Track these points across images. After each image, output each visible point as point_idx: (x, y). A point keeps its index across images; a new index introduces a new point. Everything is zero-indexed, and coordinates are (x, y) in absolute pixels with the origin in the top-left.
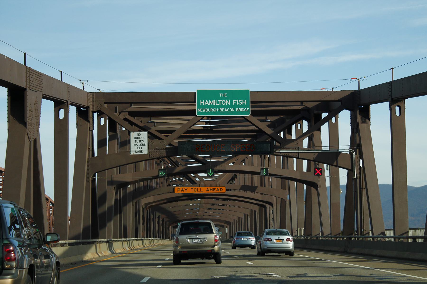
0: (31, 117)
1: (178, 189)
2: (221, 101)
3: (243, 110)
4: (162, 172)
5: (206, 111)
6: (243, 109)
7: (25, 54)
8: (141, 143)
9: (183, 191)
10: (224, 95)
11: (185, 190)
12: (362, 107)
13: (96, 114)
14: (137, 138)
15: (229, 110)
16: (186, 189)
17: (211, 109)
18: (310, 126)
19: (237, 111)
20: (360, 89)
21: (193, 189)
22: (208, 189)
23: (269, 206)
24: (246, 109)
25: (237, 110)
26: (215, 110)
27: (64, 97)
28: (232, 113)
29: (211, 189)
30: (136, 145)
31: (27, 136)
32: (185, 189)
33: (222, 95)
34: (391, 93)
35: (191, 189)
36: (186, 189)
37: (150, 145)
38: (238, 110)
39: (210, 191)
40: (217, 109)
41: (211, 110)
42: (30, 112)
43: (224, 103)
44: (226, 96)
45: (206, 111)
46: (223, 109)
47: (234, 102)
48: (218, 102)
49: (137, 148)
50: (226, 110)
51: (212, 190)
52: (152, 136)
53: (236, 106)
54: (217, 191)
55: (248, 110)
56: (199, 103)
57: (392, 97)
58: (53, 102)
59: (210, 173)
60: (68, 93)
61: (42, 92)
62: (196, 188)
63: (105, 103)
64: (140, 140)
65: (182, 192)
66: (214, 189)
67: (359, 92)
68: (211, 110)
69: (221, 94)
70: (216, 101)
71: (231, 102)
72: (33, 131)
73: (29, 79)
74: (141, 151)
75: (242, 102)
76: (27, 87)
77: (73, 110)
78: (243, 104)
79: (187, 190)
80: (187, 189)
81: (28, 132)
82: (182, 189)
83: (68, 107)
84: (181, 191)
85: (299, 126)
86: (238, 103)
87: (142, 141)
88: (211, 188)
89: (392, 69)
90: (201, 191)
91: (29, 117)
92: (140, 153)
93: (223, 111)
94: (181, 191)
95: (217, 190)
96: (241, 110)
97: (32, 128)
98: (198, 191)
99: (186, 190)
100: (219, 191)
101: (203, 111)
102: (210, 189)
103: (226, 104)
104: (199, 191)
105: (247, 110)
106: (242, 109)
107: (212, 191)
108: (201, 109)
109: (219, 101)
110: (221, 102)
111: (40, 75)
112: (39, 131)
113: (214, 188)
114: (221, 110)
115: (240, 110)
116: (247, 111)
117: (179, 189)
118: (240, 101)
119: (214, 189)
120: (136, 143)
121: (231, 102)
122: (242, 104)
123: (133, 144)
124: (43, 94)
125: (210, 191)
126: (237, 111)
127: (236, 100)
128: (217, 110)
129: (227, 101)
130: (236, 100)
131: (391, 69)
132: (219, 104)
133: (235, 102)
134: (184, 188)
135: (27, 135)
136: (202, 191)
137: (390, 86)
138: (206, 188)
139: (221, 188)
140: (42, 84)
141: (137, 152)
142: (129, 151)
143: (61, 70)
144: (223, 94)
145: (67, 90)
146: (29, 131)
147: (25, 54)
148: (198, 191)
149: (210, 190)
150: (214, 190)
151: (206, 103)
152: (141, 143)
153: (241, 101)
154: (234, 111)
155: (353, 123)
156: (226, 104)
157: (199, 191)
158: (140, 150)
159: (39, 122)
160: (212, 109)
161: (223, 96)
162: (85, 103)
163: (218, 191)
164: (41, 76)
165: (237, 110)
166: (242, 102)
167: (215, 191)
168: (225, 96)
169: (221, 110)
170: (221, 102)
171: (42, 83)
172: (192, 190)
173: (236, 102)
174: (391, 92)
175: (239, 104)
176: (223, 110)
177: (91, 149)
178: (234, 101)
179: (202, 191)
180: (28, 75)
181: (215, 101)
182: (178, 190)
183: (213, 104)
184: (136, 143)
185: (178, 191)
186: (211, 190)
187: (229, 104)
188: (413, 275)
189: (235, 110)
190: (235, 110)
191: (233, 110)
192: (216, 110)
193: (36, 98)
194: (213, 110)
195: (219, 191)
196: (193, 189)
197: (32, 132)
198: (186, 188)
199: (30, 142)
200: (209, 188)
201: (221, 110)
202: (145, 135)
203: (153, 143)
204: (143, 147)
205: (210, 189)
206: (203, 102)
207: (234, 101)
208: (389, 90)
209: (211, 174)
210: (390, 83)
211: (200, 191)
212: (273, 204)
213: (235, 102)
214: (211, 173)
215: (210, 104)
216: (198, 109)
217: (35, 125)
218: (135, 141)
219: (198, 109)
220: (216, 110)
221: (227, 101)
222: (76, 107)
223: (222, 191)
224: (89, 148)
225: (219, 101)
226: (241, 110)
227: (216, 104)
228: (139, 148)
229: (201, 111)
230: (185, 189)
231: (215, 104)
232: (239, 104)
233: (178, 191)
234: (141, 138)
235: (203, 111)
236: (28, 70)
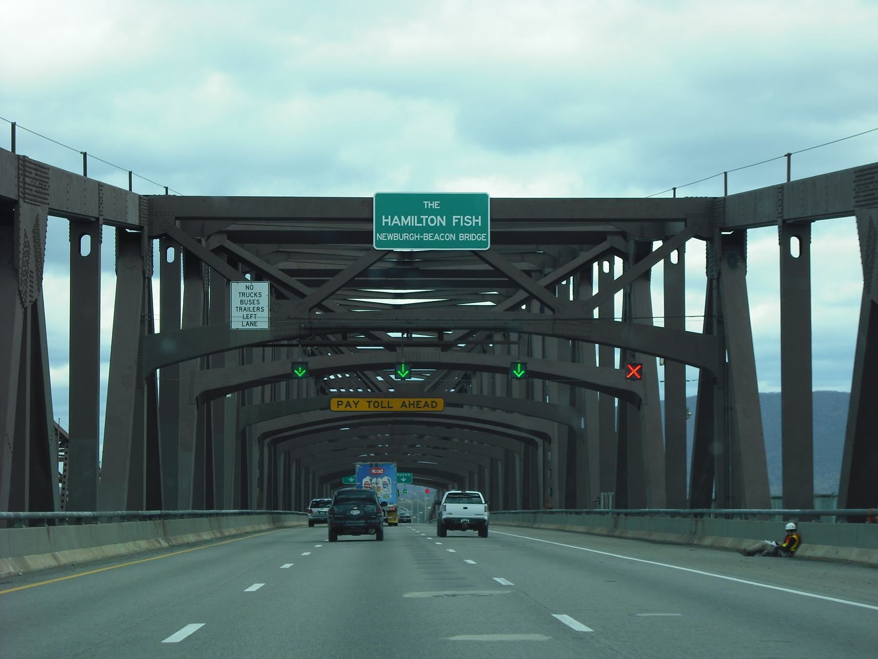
0: (27, 258)
1: (338, 402)
2: (427, 217)
3: (474, 238)
4: (300, 368)
5: (394, 239)
6: (474, 236)
7: (14, 125)
8: (254, 306)
9: (350, 406)
10: (433, 205)
11: (355, 405)
12: (730, 233)
13: (156, 243)
14: (245, 295)
15: (443, 237)
16: (356, 403)
17: (405, 234)
18: (627, 268)
19: (460, 239)
20: (729, 194)
21: (371, 402)
22: (404, 402)
23: (543, 443)
24: (481, 236)
25: (460, 237)
26: (413, 237)
27: (91, 211)
28: (451, 243)
29: (412, 402)
30: (243, 310)
31: (20, 301)
32: (354, 401)
33: (430, 205)
34: (782, 209)
35: (367, 402)
36: (356, 403)
37: (273, 309)
38: (463, 237)
39: (409, 407)
40: (417, 235)
41: (405, 237)
42: (25, 249)
43: (432, 223)
44: (437, 206)
45: (394, 239)
46: (430, 234)
47: (454, 221)
48: (420, 221)
49: (245, 316)
50: (437, 237)
51: (414, 405)
52: (276, 294)
53: (459, 229)
54: (424, 408)
55: (484, 238)
56: (379, 221)
57: (785, 218)
58: (68, 219)
59: (401, 372)
60: (99, 200)
61: (49, 204)
62: (379, 400)
63: (177, 218)
64: (252, 299)
65: (348, 409)
66: (419, 403)
67: (723, 202)
68: (405, 237)
69: (428, 204)
70: (416, 217)
71: (449, 221)
72: (30, 291)
73: (24, 180)
74: (254, 324)
75: (471, 220)
76: (19, 197)
77: (109, 233)
78: (474, 225)
79: (357, 405)
80: (358, 401)
81: (21, 288)
82: (348, 402)
83: (100, 231)
84: (345, 407)
85: (606, 264)
86: (464, 221)
87: (256, 302)
88: (412, 400)
89: (789, 156)
90: (389, 407)
91: (23, 259)
92: (252, 327)
93: (430, 239)
94: (345, 407)
95: (425, 406)
96: (470, 237)
97: (28, 280)
98: (382, 407)
99: (356, 404)
100: (429, 407)
101: (389, 239)
102: (409, 402)
103: (438, 225)
104: (386, 407)
105: (482, 238)
106: (473, 234)
107: (414, 407)
108: (383, 234)
109: (422, 217)
110: (427, 219)
111: (41, 169)
112: (41, 286)
113: (417, 402)
114: (426, 238)
115: (468, 237)
116: (483, 240)
117: (341, 403)
118: (467, 219)
119: (419, 403)
120: (243, 306)
121: (449, 221)
122: (472, 224)
123: (240, 293)
124: (49, 208)
125: (409, 407)
126: (460, 239)
127: (459, 217)
128: (418, 237)
129: (438, 217)
130: (459, 217)
131: (786, 156)
132: (421, 225)
133: (457, 221)
134: (351, 400)
135: (19, 296)
136: (392, 407)
137: (781, 194)
138: (402, 400)
139: (434, 402)
140: (49, 187)
141: (245, 324)
142: (229, 324)
143: (84, 151)
144: (431, 203)
145: (98, 200)
146: (22, 288)
147: (14, 125)
148: (382, 407)
149: (410, 404)
150: (419, 406)
151: (394, 222)
152: (254, 306)
153: (470, 218)
154: (454, 239)
155: (711, 268)
156: (438, 225)
157: (386, 407)
158: (253, 320)
159: (43, 268)
160: (406, 235)
161: (432, 206)
162: (133, 218)
163: (426, 409)
164: (47, 171)
165: (462, 238)
166: (471, 220)
167: (421, 407)
168: (436, 207)
169: (427, 237)
170: (427, 219)
171: (47, 185)
172: (369, 404)
173: (459, 219)
174: (781, 208)
175: (465, 224)
176: (431, 238)
177: (147, 317)
178: (454, 217)
179: (392, 407)
180: (21, 172)
181: (413, 217)
182: (338, 405)
183: (409, 225)
184: (243, 306)
185: (338, 407)
186: (412, 406)
187: (444, 225)
188: (747, 584)
189: (457, 237)
190: (457, 237)
191: (452, 237)
192: (416, 237)
193: (37, 217)
194: (409, 237)
195: (429, 407)
196: (371, 402)
197: (29, 288)
198: (356, 400)
199: (26, 309)
200: (407, 401)
201: (427, 237)
202: (263, 288)
203: (282, 306)
204: (259, 314)
205: (409, 402)
206: (389, 220)
207: (454, 217)
208: (778, 203)
209: (405, 374)
210: (780, 188)
211: (387, 406)
212: (550, 439)
213: (457, 221)
214: (405, 371)
215: (402, 225)
216: (378, 234)
217: (34, 275)
218: (242, 302)
219: (378, 234)
220: (416, 237)
221: (438, 217)
222: (115, 228)
223: (436, 406)
224: (142, 315)
225: (423, 218)
226: (469, 237)
227: (416, 225)
228: (251, 317)
229: (384, 238)
230: (354, 401)
231: (413, 225)
232: (465, 224)
233: (338, 407)
234: (255, 295)
235: (389, 239)
236: (20, 161)
